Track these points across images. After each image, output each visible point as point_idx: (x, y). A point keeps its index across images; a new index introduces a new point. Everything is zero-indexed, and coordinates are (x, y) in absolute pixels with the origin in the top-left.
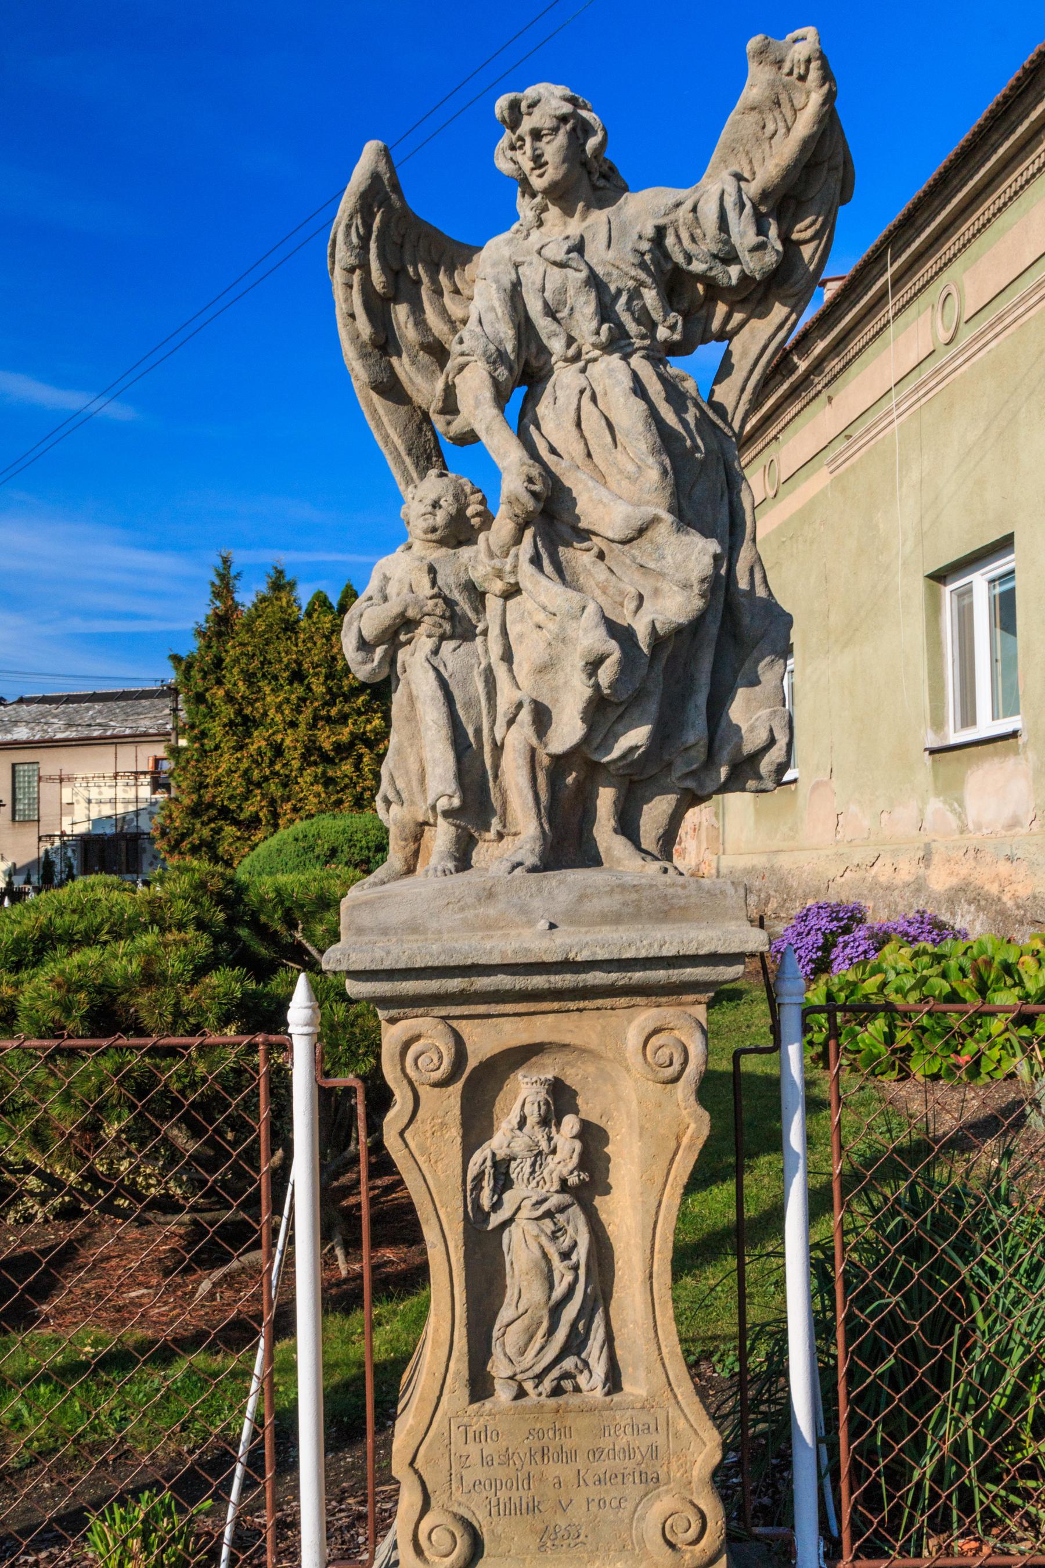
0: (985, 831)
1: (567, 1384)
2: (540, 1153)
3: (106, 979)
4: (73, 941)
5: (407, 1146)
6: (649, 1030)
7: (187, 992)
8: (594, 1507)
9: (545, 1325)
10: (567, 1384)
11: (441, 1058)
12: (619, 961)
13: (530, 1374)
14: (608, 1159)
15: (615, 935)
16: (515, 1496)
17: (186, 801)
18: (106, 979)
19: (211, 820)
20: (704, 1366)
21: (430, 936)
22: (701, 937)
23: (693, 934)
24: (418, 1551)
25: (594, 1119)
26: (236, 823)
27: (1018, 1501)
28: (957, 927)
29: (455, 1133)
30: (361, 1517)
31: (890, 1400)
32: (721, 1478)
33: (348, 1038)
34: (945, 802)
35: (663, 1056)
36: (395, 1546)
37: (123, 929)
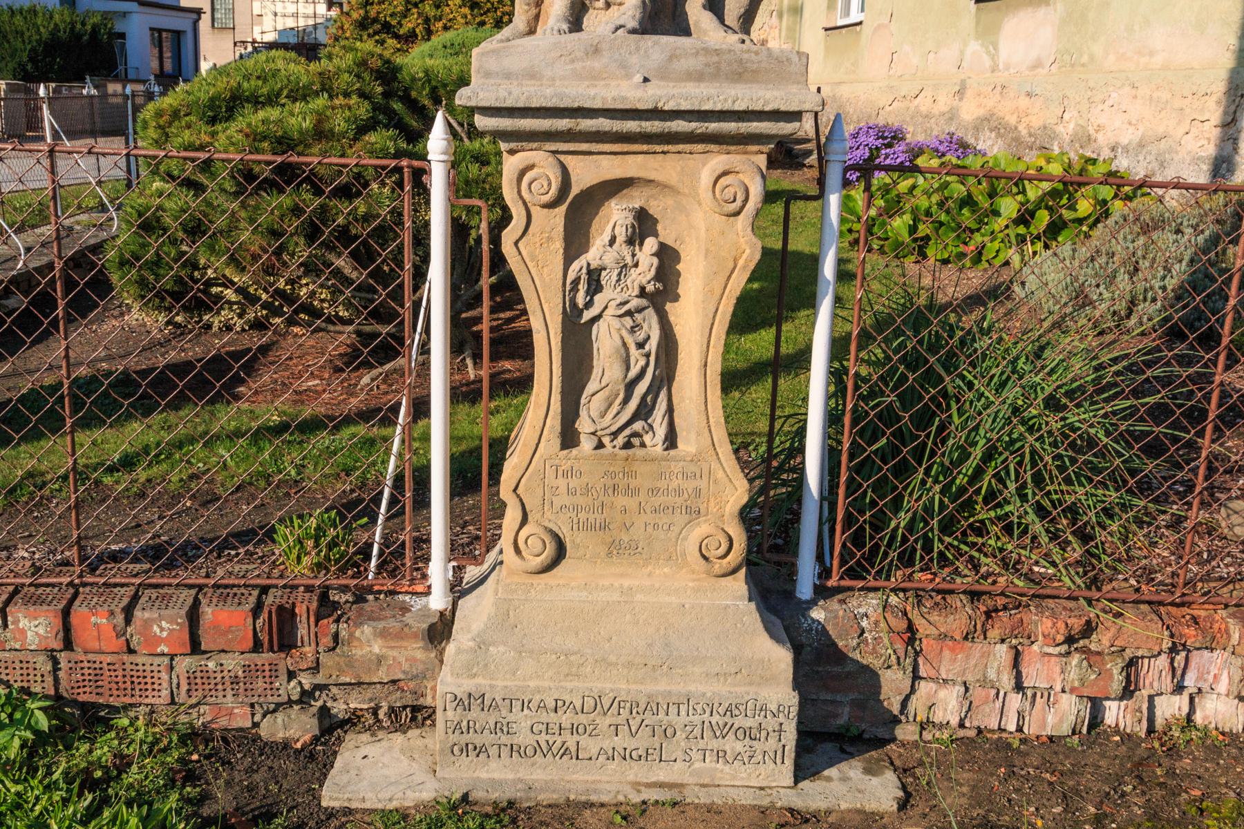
0: (1012, 71)
1: (636, 441)
2: (625, 266)
3: (285, 132)
4: (257, 102)
5: (520, 253)
6: (716, 175)
7: (351, 147)
8: (650, 529)
9: (621, 396)
10: (636, 441)
11: (550, 184)
12: (699, 112)
13: (608, 431)
14: (679, 274)
15: (697, 91)
16: (592, 517)
17: (355, 15)
18: (285, 132)
19: (376, 33)
20: (742, 452)
21: (544, 82)
22: (767, 96)
23: (761, 93)
24: (517, 550)
25: (670, 242)
26: (397, 36)
27: (967, 549)
28: (978, 148)
29: (558, 245)
30: (477, 538)
31: (881, 469)
32: (744, 515)
33: (476, 180)
34: (982, 45)
35: (729, 194)
36: (501, 552)
37: (300, 94)
